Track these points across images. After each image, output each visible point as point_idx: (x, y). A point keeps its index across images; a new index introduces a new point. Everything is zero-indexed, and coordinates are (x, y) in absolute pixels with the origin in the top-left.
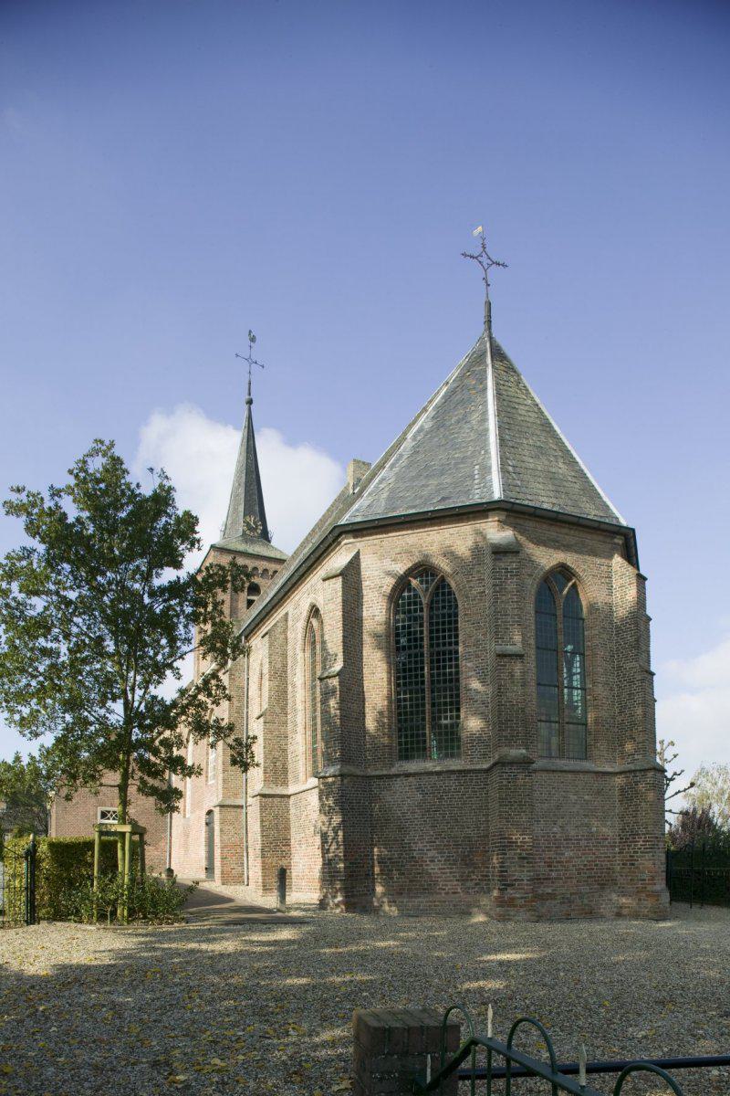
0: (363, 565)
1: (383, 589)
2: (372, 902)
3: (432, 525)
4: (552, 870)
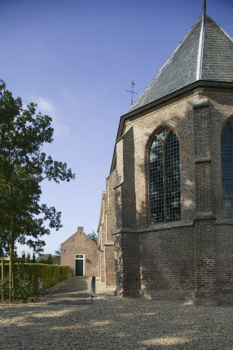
0: (134, 133)
1: (143, 143)
2: (139, 292)
3: (165, 105)
4: (231, 278)
